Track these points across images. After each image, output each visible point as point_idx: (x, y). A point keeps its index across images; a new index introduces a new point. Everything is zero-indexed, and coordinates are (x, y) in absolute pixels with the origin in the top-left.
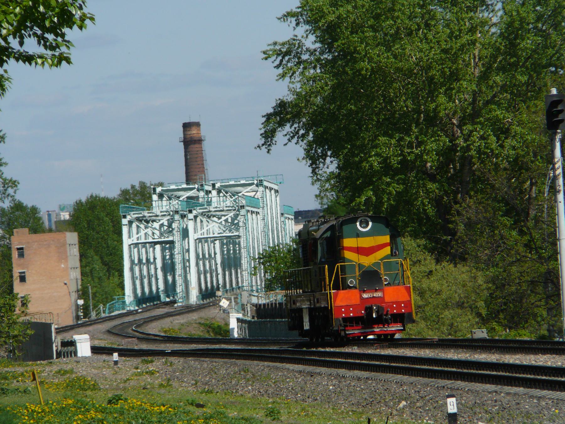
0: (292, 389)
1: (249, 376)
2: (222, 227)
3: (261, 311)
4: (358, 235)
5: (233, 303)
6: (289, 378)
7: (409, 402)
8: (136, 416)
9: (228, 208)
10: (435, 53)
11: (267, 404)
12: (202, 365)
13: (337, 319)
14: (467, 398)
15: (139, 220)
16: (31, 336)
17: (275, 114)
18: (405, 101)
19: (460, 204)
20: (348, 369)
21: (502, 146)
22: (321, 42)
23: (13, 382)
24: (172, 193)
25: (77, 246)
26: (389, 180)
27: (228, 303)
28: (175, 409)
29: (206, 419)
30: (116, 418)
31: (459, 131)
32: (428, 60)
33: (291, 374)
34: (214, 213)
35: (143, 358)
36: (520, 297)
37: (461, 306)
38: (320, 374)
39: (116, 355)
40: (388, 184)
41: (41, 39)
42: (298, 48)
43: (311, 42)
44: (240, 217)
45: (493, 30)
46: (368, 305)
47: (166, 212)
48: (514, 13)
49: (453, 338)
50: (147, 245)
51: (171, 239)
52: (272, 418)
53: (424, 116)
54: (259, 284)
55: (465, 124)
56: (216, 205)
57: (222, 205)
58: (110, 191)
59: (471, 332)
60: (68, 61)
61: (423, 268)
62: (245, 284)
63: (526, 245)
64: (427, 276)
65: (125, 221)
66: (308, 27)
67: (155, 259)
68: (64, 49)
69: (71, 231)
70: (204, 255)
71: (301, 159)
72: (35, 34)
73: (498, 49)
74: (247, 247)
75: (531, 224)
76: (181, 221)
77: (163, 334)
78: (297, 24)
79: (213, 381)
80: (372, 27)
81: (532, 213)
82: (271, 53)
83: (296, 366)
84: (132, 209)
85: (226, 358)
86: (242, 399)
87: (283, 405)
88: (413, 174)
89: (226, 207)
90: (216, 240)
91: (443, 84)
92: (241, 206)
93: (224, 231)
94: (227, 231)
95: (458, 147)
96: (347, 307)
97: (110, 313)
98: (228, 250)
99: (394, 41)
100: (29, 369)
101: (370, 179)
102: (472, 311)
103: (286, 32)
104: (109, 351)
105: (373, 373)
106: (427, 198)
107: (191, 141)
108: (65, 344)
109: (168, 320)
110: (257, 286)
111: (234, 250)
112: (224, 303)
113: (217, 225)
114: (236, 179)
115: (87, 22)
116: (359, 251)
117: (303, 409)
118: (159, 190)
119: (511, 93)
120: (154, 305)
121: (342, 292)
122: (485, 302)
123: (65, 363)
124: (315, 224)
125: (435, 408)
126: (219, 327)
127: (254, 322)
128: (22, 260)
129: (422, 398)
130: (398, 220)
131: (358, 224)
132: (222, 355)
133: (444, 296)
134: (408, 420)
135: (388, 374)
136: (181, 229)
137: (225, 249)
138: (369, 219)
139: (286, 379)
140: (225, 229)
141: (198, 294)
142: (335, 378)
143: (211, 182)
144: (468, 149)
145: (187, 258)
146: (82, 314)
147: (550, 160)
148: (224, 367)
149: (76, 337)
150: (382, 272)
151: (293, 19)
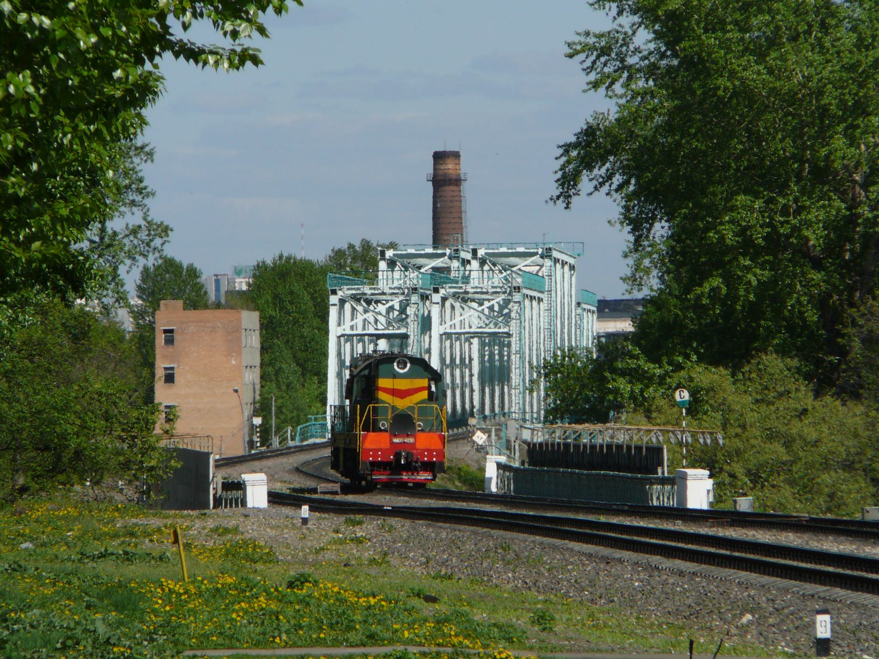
0: (576, 581)
1: (511, 556)
2: (483, 318)
3: (536, 454)
4: (395, 376)
6: (572, 563)
7: (757, 616)
8: (330, 611)
9: (494, 290)
11: (535, 603)
12: (437, 535)
13: (364, 462)
14: (849, 615)
16: (176, 470)
18: (781, 141)
19: (858, 308)
23: (144, 542)
24: (409, 261)
25: (258, 333)
26: (748, 263)
28: (391, 602)
30: (299, 611)
31: (863, 194)
32: (820, 80)
35: (348, 516)
37: (849, 466)
38: (620, 561)
39: (305, 508)
40: (748, 269)
42: (621, 46)
43: (643, 38)
44: (512, 304)
47: (399, 288)
51: (403, 331)
52: (541, 627)
53: (809, 167)
54: (535, 410)
56: (476, 284)
57: (487, 285)
58: (317, 253)
59: (863, 509)
61: (793, 404)
62: (513, 410)
65: (334, 299)
66: (636, 19)
69: (248, 309)
70: (453, 360)
74: (521, 352)
76: (421, 304)
78: (620, 13)
80: (736, 23)
83: (585, 546)
85: (556, 538)
87: (559, 607)
89: (493, 287)
90: (473, 337)
91: (842, 119)
93: (487, 325)
94: (492, 325)
95: (859, 218)
96: (375, 451)
97: (302, 440)
98: (492, 355)
99: (769, 48)
101: (719, 259)
102: (866, 475)
105: (703, 566)
106: (805, 294)
107: (445, 182)
110: (532, 412)
111: (501, 355)
112: (480, 438)
113: (476, 314)
114: (511, 245)
116: (394, 392)
117: (591, 615)
118: (389, 253)
121: (372, 435)
123: (227, 517)
125: (797, 628)
127: (525, 470)
128: (170, 349)
129: (777, 610)
130: (759, 326)
131: (395, 364)
133: (823, 449)
134: (753, 644)
135: (727, 570)
137: (487, 353)
139: (567, 565)
140: (487, 322)
142: (644, 569)
143: (471, 247)
149: (246, 477)
150: (416, 416)
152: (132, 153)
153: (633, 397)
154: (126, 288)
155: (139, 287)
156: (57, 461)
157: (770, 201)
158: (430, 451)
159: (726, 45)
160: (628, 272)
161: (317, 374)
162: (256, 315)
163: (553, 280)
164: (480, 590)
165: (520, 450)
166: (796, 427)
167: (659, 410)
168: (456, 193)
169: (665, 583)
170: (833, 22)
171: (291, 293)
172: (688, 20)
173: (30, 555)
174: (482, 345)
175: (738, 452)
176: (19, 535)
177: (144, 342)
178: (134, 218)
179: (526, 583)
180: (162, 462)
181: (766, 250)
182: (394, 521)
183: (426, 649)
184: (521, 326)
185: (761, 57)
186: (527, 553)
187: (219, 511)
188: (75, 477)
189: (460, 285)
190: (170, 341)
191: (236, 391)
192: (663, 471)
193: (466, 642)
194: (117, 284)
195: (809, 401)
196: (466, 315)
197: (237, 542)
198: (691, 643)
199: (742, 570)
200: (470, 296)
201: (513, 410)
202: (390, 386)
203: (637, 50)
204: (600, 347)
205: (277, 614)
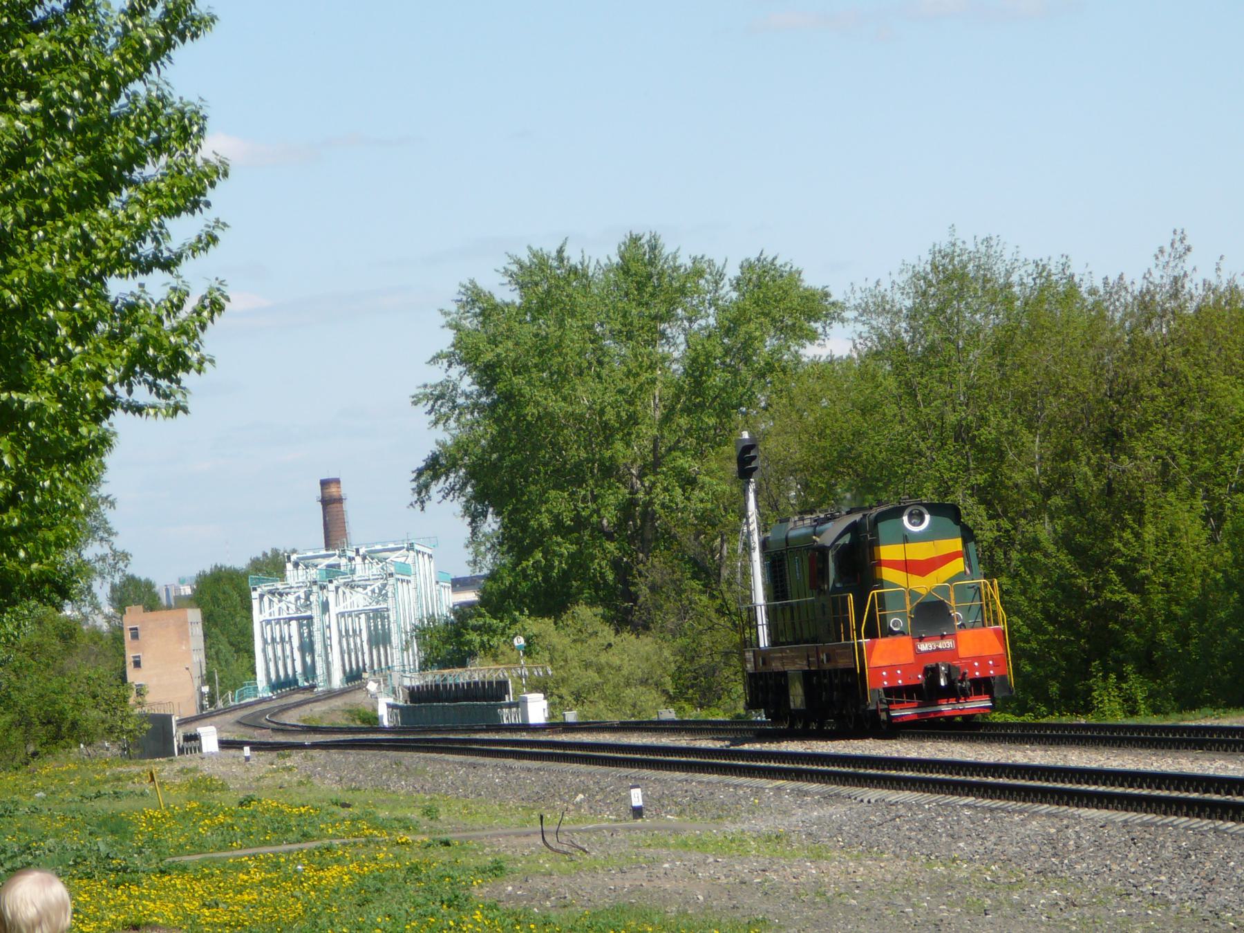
1: (403, 769)
3: (416, 695)
4: (906, 538)
10: (610, 397)
15: (272, 593)
16: (147, 731)
17: (427, 467)
21: (688, 499)
22: (478, 383)
27: (376, 685)
29: (353, 820)
36: (712, 671)
41: (153, 386)
43: (467, 384)
45: (674, 366)
46: (929, 665)
48: (699, 347)
51: (309, 613)
55: (646, 475)
58: (240, 562)
60: (185, 411)
61: (602, 641)
63: (717, 611)
65: (255, 595)
66: (462, 368)
67: (290, 637)
68: (179, 397)
70: (347, 631)
72: (146, 381)
73: (681, 389)
75: (724, 587)
78: (450, 366)
81: (725, 573)
84: (261, 581)
86: (394, 797)
88: (587, 532)
96: (891, 668)
98: (376, 626)
100: (145, 768)
101: (539, 539)
103: (437, 374)
104: (239, 745)
107: (330, 502)
108: (188, 738)
109: (307, 708)
111: (383, 625)
112: (372, 687)
114: (384, 543)
115: (207, 365)
116: (908, 566)
118: (294, 557)
121: (882, 643)
122: (673, 676)
127: (408, 707)
128: (136, 643)
131: (905, 518)
133: (625, 672)
138: (924, 510)
144: (651, 503)
147: (743, 514)
148: (374, 760)
150: (953, 604)
151: (445, 361)
153: (482, 645)
156: (59, 730)
157: (572, 494)
158: (982, 660)
159: (529, 383)
160: (471, 558)
161: (247, 651)
166: (603, 658)
167: (503, 653)
169: (518, 778)
171: (224, 593)
172: (500, 367)
174: (368, 618)
175: (563, 680)
177: (117, 639)
178: (104, 550)
183: (346, 840)
187: (182, 757)
188: (72, 742)
190: (135, 636)
192: (509, 698)
193: (375, 832)
195: (612, 639)
198: (542, 817)
202: (901, 557)
204: (455, 612)
205: (232, 826)
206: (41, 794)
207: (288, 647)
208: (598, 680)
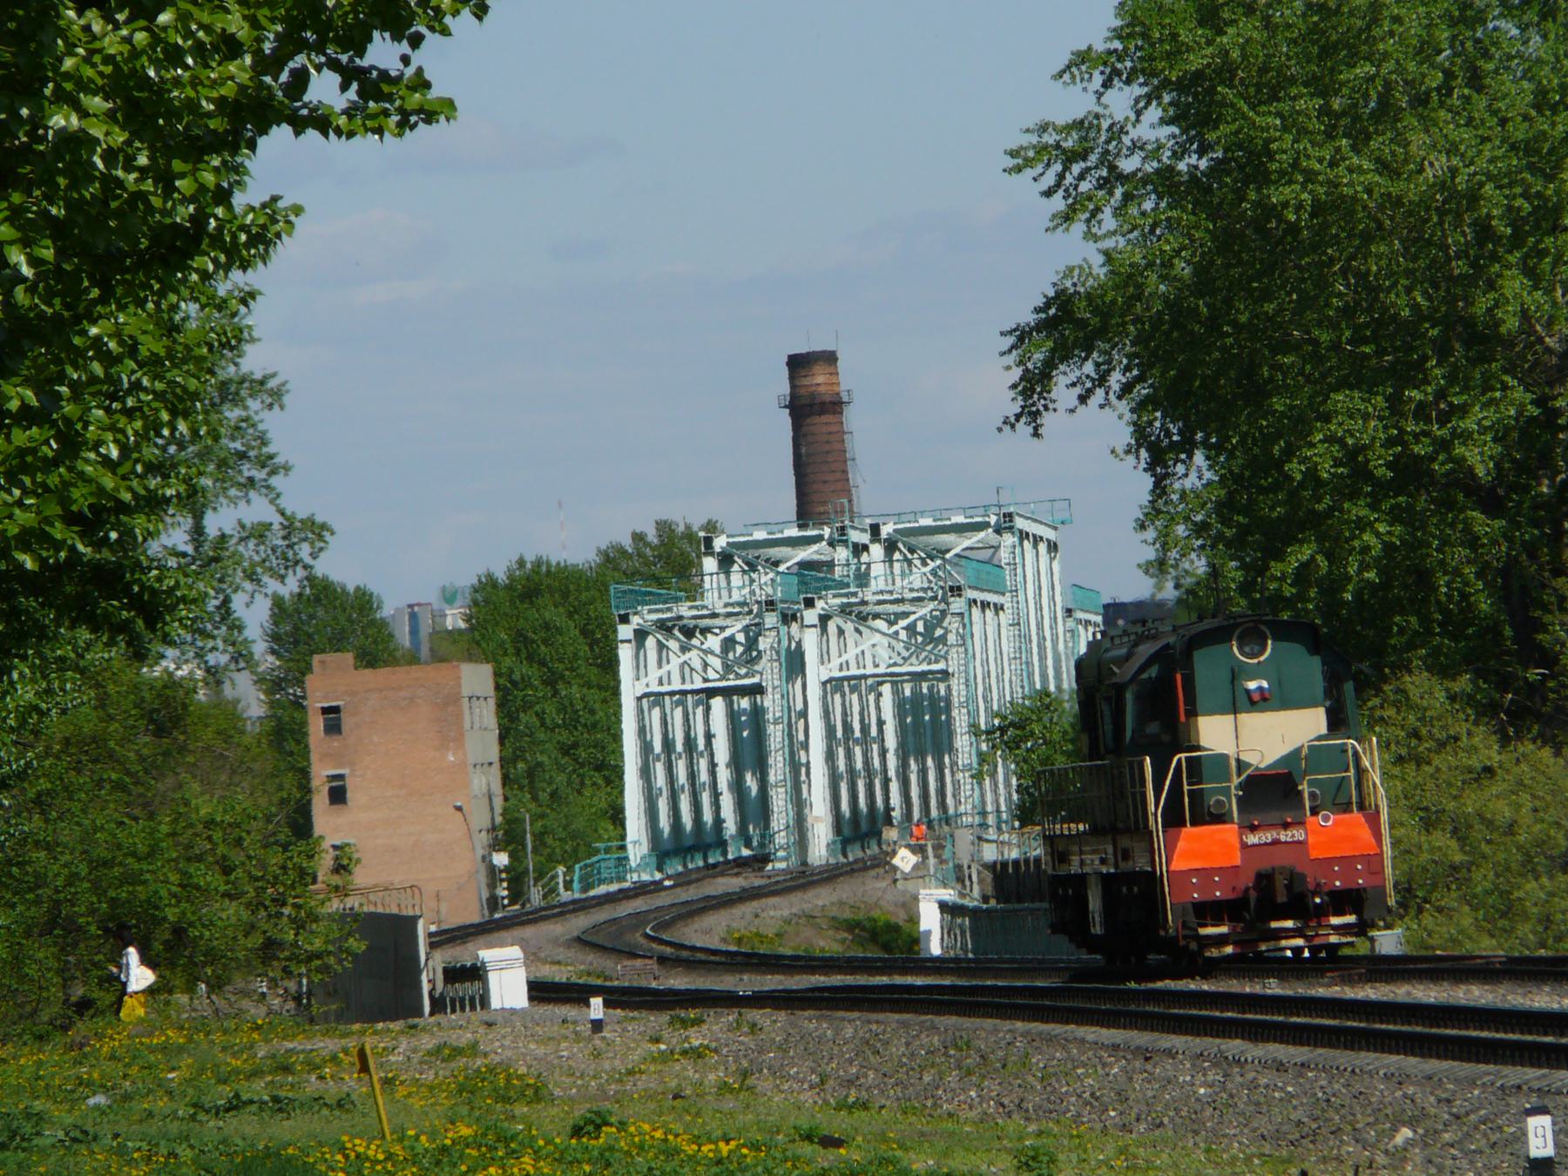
0: (1092, 1095)
3: (1005, 878)
5: (932, 861)
6: (1084, 1065)
15: (664, 627)
20: (1250, 1040)
25: (492, 703)
33: (1089, 1059)
34: (879, 609)
38: (1170, 1053)
39: (597, 1002)
42: (1108, 142)
43: (1152, 128)
47: (743, 604)
49: (1550, 953)
50: (667, 698)
56: (882, 586)
64: (1476, 780)
65: (625, 632)
67: (709, 737)
70: (668, 744)
71: (1120, 450)
74: (970, 700)
77: (733, 948)
78: (1107, 84)
79: (871, 1074)
82: (1031, 154)
83: (1104, 1031)
90: (881, 683)
92: (952, 589)
97: (585, 889)
100: (352, 1043)
103: (1074, 102)
104: (576, 994)
105: (1320, 1051)
107: (812, 406)
108: (454, 974)
109: (748, 908)
110: (998, 811)
112: (905, 860)
113: (885, 641)
118: (720, 543)
119: (1396, 350)
120: (708, 867)
123: (458, 1028)
124: (1117, 641)
126: (894, 929)
128: (335, 743)
129: (1458, 1117)
132: (897, 1001)
135: (1363, 1054)
136: (783, 653)
140: (906, 654)
141: (830, 836)
142: (1215, 1065)
143: (868, 521)
145: (801, 737)
146: (506, 893)
149: (487, 955)
152: (243, 393)
154: (248, 633)
155: (275, 637)
160: (1150, 553)
162: (486, 670)
163: (1019, 570)
164: (920, 1123)
165: (980, 881)
168: (834, 428)
169: (1253, 1086)
170: (1490, 66)
173: (103, 1113)
176: (80, 1084)
177: (286, 733)
178: (258, 510)
179: (1002, 1105)
180: (333, 942)
181: (1397, 486)
182: (755, 1015)
184: (969, 657)
185: (1360, 141)
186: (1001, 1054)
189: (852, 589)
190: (333, 728)
191: (459, 809)
194: (230, 628)
195: (1491, 753)
196: (865, 646)
197: (478, 1071)
199: (1391, 1053)
200: (869, 608)
201: (962, 809)
203: (1136, 146)
206: (100, 1099)
207: (703, 764)
208: (1458, 858)
